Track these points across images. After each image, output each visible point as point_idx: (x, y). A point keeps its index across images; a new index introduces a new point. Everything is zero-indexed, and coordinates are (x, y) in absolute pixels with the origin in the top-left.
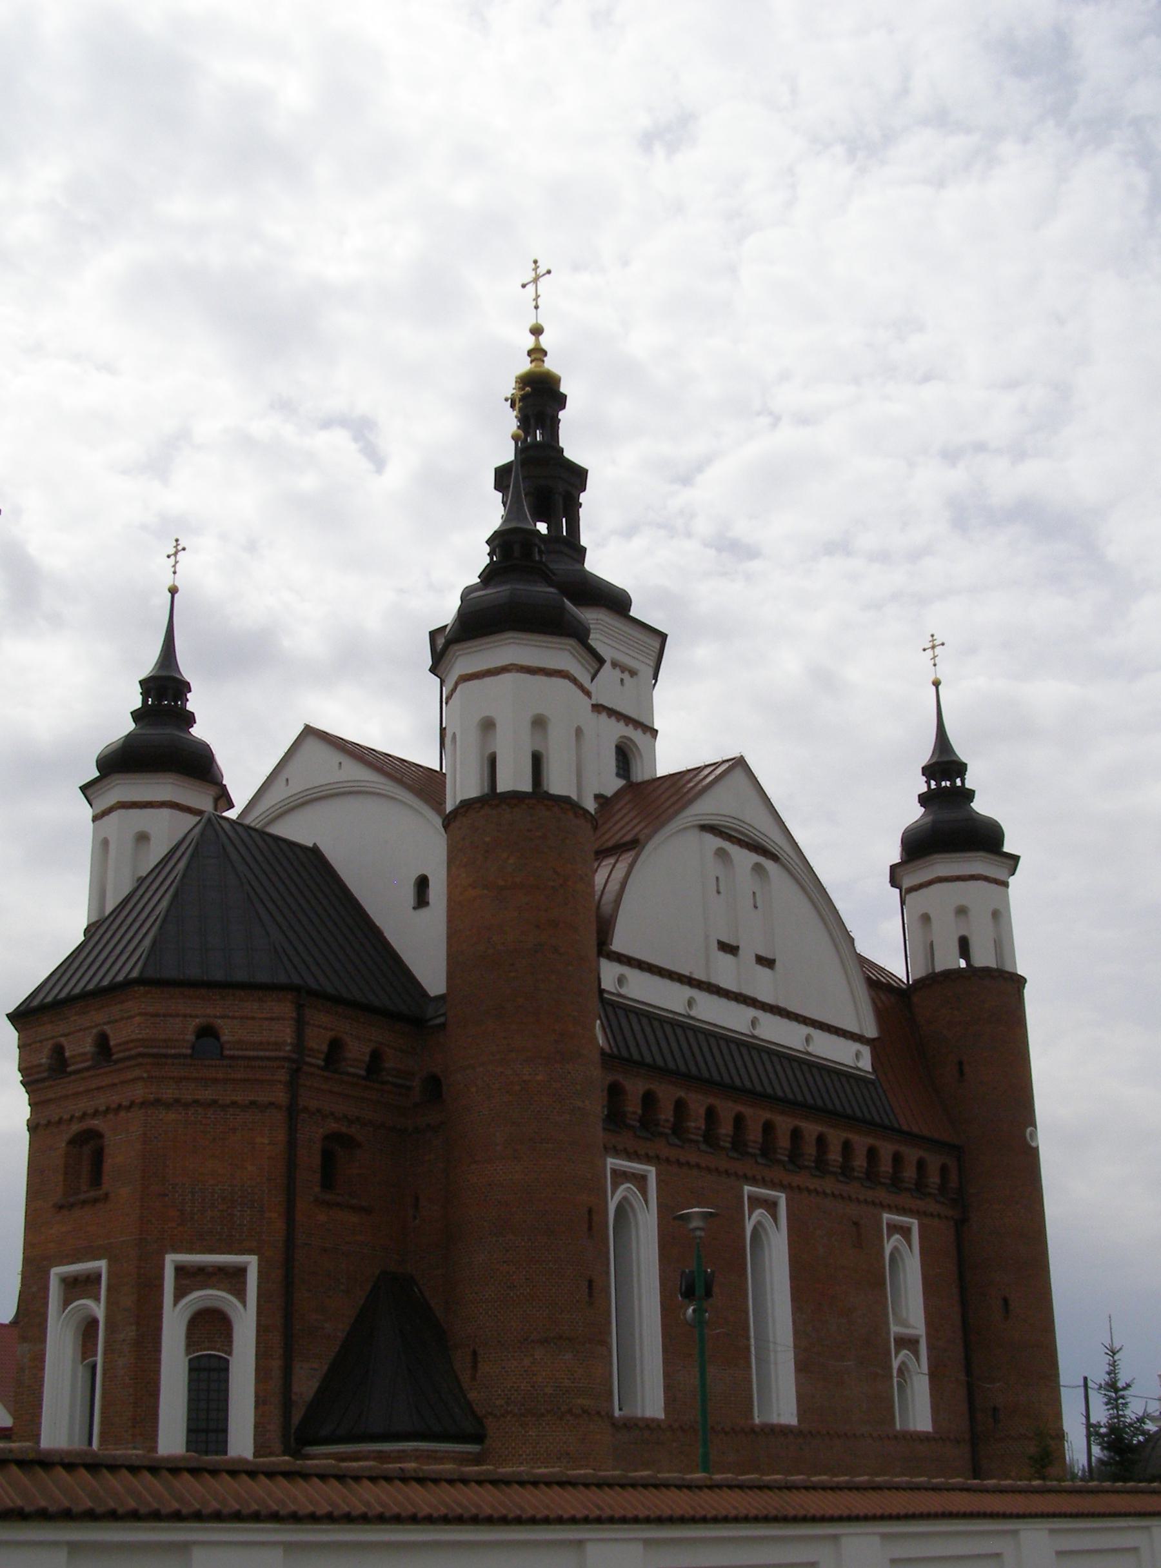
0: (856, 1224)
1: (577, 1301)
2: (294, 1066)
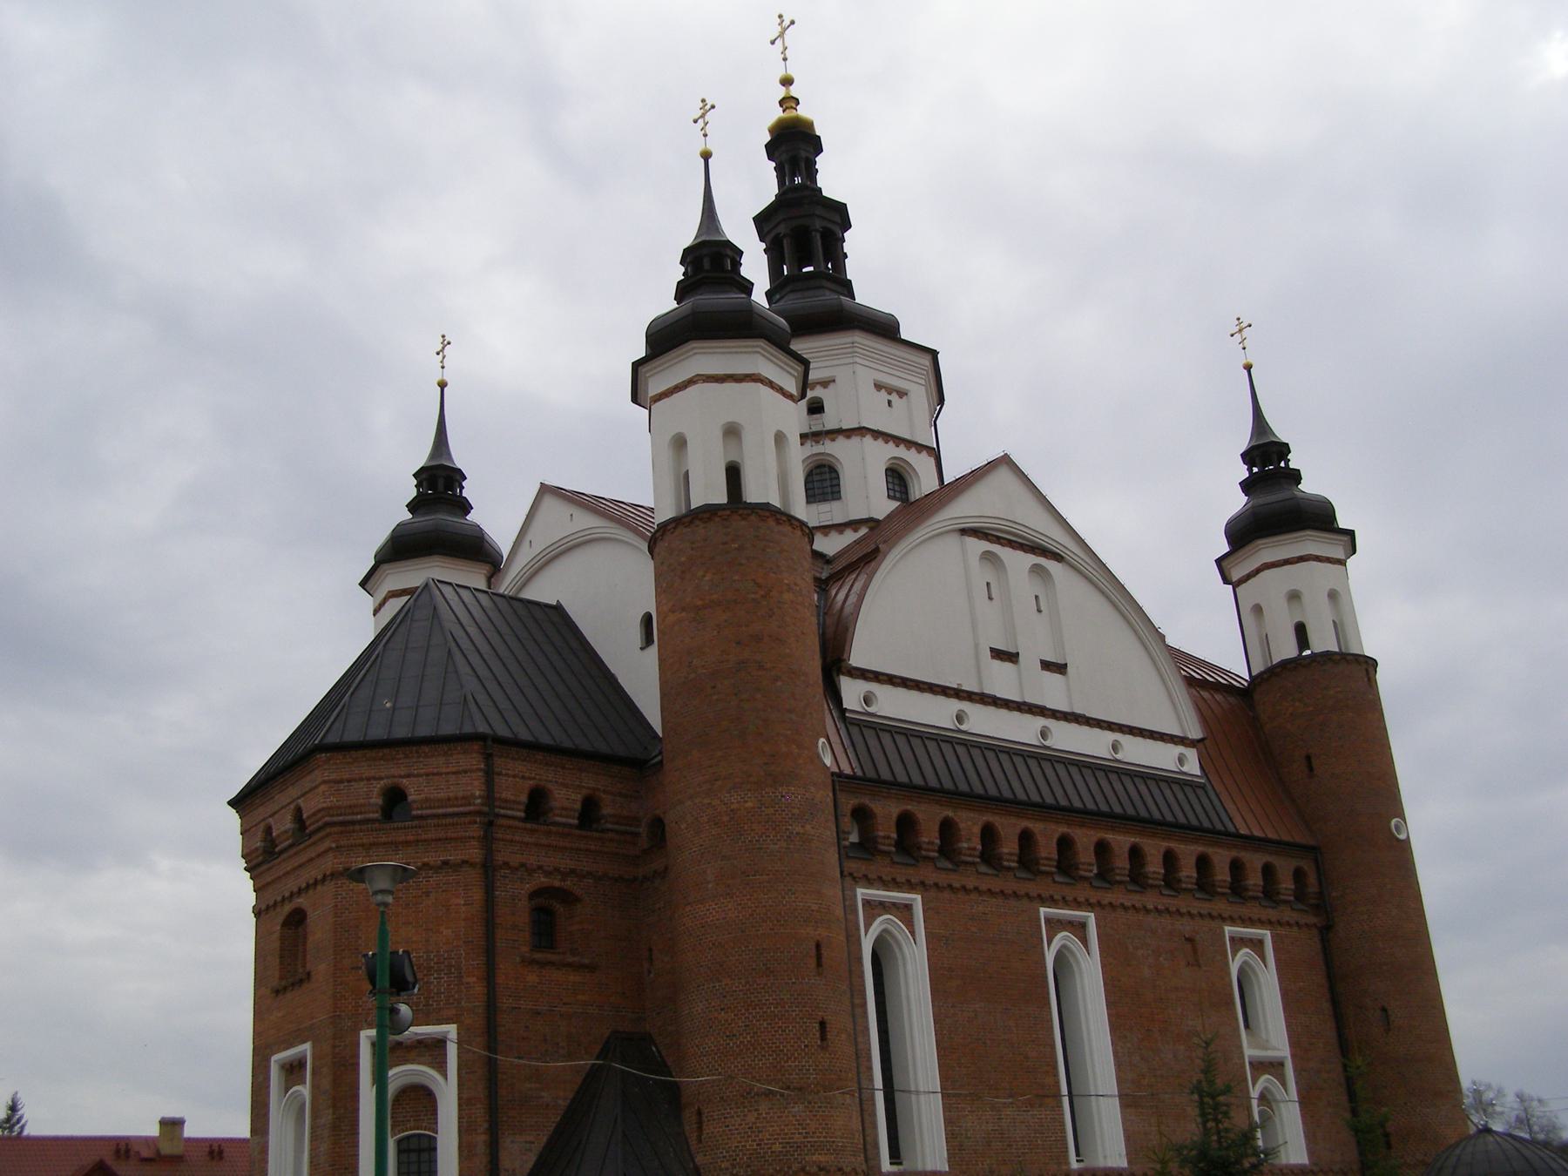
0: (1190, 940)
1: (806, 1046)
2: (486, 820)
